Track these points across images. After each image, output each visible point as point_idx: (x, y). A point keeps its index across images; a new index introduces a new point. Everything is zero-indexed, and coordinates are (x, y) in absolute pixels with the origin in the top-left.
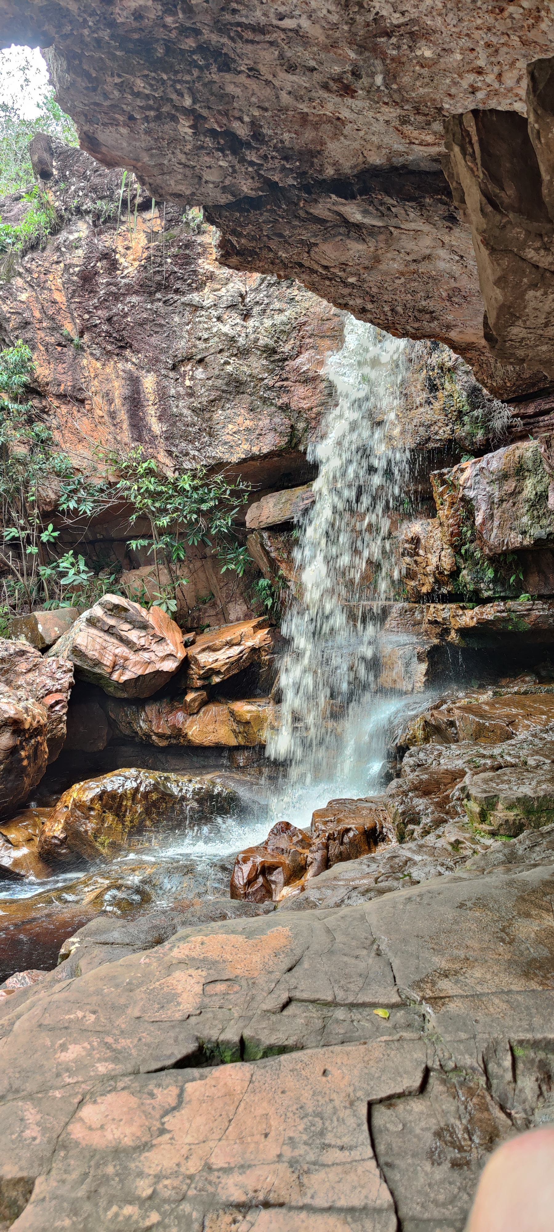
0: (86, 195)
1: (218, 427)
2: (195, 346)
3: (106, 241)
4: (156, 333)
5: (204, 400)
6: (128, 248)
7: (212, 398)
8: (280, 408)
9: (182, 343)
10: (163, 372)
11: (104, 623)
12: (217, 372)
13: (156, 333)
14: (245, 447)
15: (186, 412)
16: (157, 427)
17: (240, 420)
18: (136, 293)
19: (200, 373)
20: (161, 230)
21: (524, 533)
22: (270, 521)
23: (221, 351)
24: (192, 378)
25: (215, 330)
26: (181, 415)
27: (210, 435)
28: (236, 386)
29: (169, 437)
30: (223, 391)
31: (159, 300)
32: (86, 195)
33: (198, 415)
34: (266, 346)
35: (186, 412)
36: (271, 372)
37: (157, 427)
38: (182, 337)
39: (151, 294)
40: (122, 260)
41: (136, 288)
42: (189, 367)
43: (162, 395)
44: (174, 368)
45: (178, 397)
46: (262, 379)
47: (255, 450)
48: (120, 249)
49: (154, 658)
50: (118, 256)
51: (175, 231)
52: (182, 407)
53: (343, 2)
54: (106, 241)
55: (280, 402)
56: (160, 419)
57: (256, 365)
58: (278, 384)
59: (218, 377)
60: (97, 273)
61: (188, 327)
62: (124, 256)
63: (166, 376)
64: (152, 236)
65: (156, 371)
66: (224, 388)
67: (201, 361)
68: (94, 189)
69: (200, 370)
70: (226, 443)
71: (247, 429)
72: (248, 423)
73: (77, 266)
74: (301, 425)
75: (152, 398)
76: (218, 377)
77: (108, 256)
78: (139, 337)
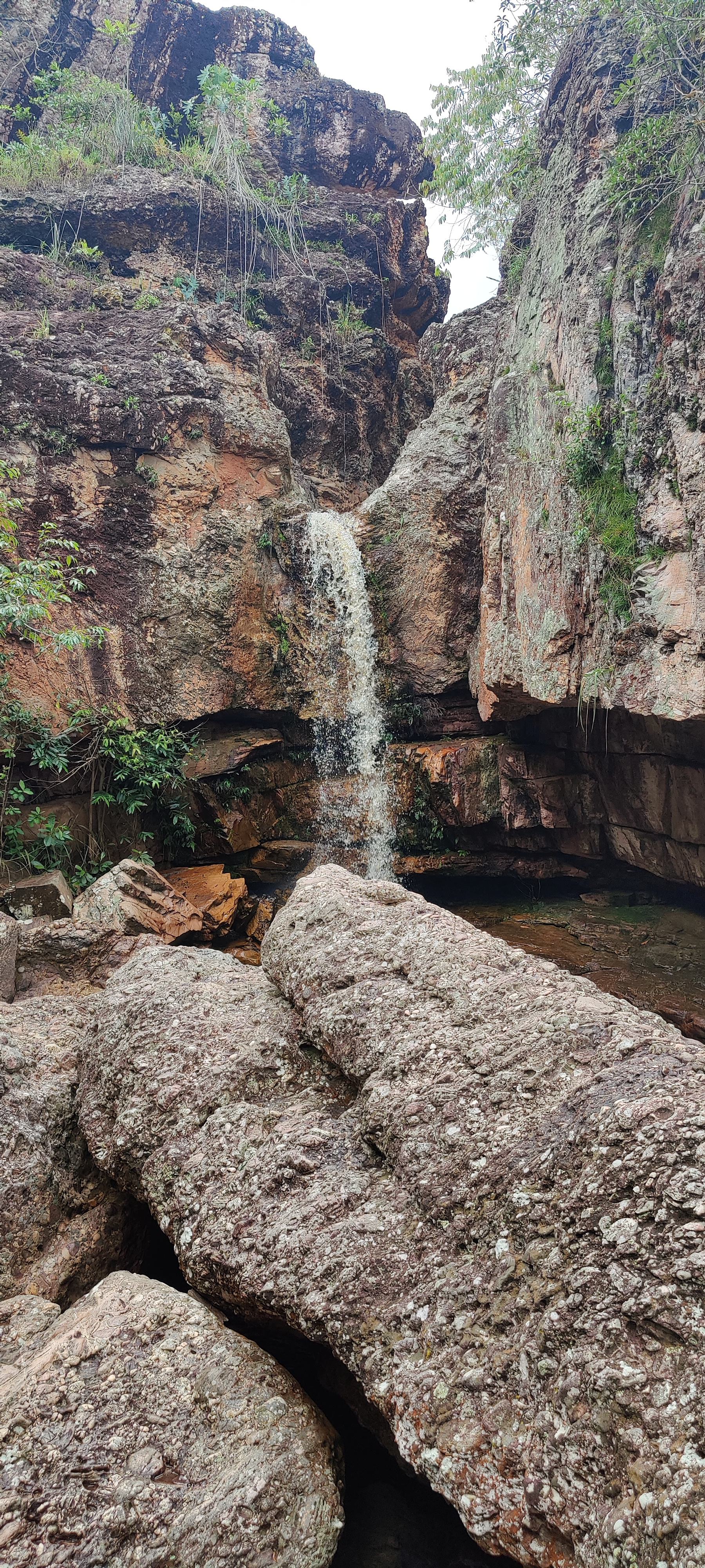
0: (35, 419)
1: (177, 684)
2: (160, 605)
3: (59, 474)
4: (121, 585)
5: (167, 659)
6: (81, 487)
7: (174, 657)
8: (225, 670)
9: (148, 600)
10: (129, 626)
11: (136, 890)
12: (179, 633)
13: (121, 585)
14: (200, 706)
15: (150, 669)
16: (121, 682)
17: (195, 679)
18: (98, 539)
19: (161, 630)
20: (112, 475)
21: (485, 813)
22: (207, 772)
23: (182, 612)
24: (154, 635)
25: (174, 591)
26: (146, 671)
27: (170, 692)
28: (191, 647)
29: (133, 693)
30: (183, 651)
31: (120, 551)
32: (35, 419)
33: (160, 672)
34: (217, 612)
35: (150, 669)
36: (219, 636)
37: (121, 682)
38: (148, 595)
39: (112, 543)
40: (77, 499)
41: (98, 534)
42: (151, 625)
43: (128, 648)
44: (138, 624)
45: (142, 653)
46: (213, 642)
47: (208, 709)
48: (75, 487)
49: (182, 919)
50: (73, 495)
51: (128, 479)
52: (145, 663)
53: (704, 652)
54: (59, 474)
55: (225, 664)
56: (124, 673)
57: (205, 628)
58: (224, 648)
59: (180, 638)
60: (50, 507)
61: (153, 585)
62: (79, 495)
63: (130, 631)
64: (103, 478)
65: (121, 625)
66: (184, 648)
67: (162, 621)
68: (45, 415)
69: (162, 628)
70: (184, 701)
71: (201, 689)
72: (202, 683)
73: (30, 496)
74: (240, 686)
75: (117, 652)
76: (180, 638)
77: (63, 492)
78: (103, 587)
